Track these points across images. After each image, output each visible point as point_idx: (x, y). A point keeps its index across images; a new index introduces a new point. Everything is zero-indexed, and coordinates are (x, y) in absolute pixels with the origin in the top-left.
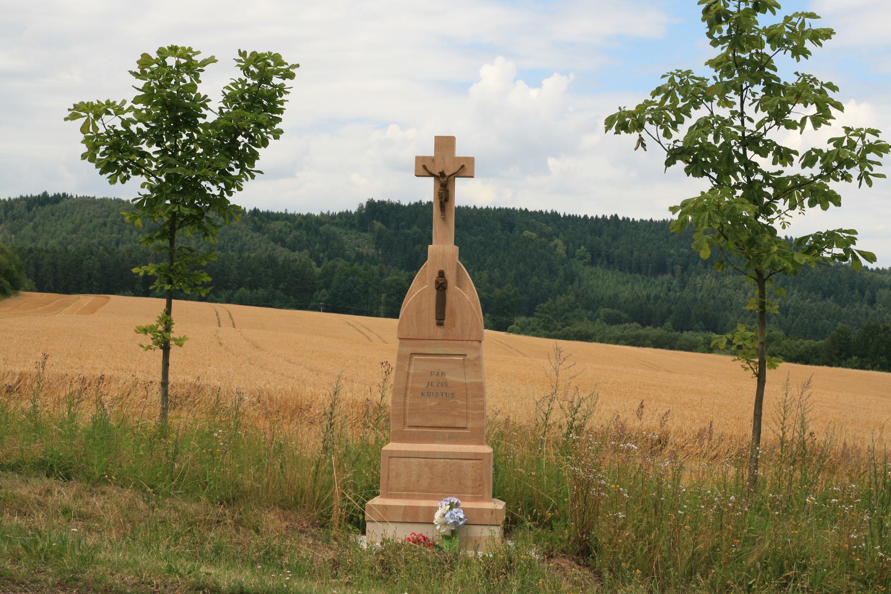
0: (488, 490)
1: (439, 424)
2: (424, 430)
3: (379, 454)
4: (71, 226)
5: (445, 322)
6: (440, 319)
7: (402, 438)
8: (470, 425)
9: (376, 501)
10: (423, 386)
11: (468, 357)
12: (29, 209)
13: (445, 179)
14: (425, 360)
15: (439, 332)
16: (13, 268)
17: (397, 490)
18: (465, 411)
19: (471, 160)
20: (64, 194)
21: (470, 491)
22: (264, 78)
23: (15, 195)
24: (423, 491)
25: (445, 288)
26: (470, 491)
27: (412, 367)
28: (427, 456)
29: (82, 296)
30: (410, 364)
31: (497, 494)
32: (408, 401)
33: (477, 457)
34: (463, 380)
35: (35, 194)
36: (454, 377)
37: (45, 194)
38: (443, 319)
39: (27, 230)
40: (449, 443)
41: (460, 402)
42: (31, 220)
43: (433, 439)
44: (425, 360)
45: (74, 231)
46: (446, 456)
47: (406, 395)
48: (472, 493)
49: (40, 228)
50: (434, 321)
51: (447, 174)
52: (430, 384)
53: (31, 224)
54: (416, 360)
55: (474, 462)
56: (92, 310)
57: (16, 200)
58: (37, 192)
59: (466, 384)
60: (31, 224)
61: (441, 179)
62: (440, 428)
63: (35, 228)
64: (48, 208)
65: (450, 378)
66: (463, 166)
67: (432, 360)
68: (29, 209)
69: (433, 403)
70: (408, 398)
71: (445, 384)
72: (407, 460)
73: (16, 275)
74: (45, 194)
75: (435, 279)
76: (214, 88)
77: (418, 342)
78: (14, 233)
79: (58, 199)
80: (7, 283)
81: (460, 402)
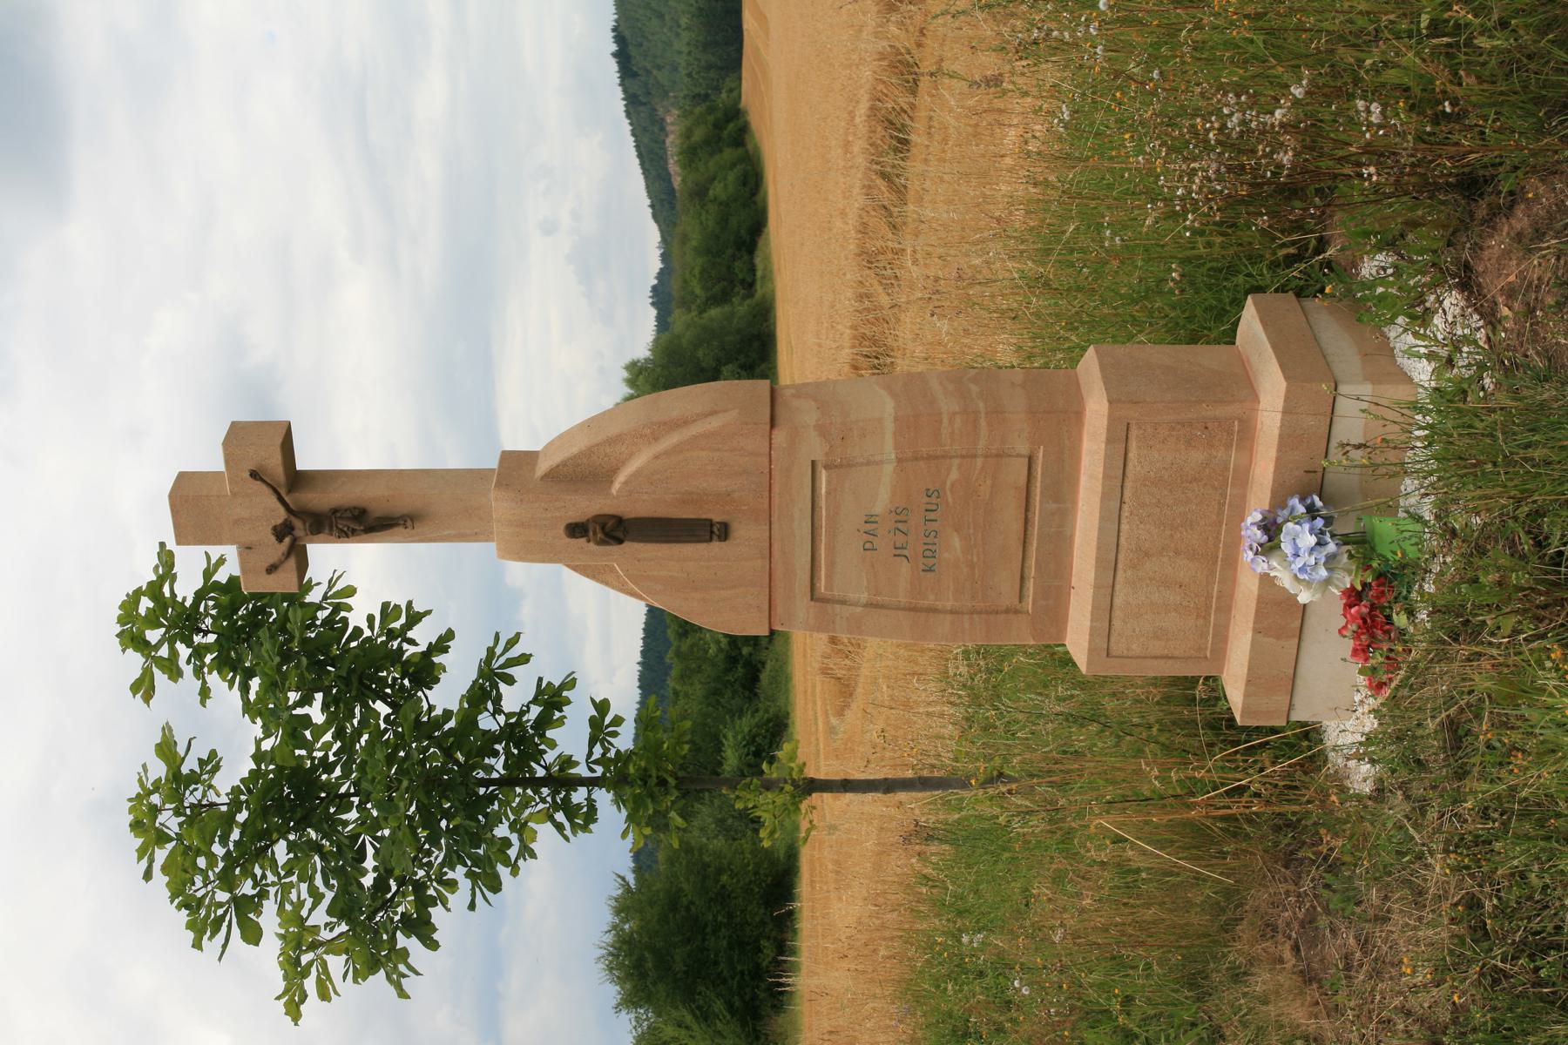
0: (1208, 356)
1: (1017, 526)
2: (1032, 562)
3: (1102, 681)
4: (655, 22)
5: (716, 518)
6: (712, 531)
7: (1055, 613)
8: (1023, 448)
9: (1235, 696)
10: (905, 568)
11: (819, 456)
12: (635, 75)
13: (297, 523)
14: (831, 565)
15: (746, 533)
16: (711, 118)
17: (1204, 635)
18: (979, 462)
19: (238, 436)
20: (614, 30)
21: (1221, 454)
22: (185, 622)
23: (619, 93)
24: (1213, 573)
25: (620, 521)
26: (1221, 454)
27: (851, 596)
28: (1109, 565)
29: (745, 26)
30: (843, 602)
31: (1217, 325)
32: (948, 605)
33: (1113, 377)
34: (889, 469)
35: (615, 67)
36: (880, 490)
37: (614, 55)
38: (711, 523)
39: (662, 77)
40: (1074, 502)
41: (954, 475)
42: (649, 72)
43: (1059, 545)
44: (831, 565)
45: (661, 16)
46: (1113, 515)
47: (933, 610)
48: (1229, 446)
49: (658, 61)
50: (716, 546)
51: (281, 515)
52: (899, 552)
53: (655, 72)
54: (829, 587)
55: (1133, 445)
56: (762, 18)
57: (625, 91)
58: (613, 66)
59: (899, 461)
60: (655, 72)
61: (299, 532)
62: (1027, 521)
63: (659, 68)
64: (633, 51)
65: (882, 502)
66: (254, 475)
67: (831, 550)
68: (635, 75)
69: (956, 542)
70: (939, 604)
71: (900, 514)
72: (1117, 613)
73: (719, 114)
74: (614, 55)
75: (592, 546)
76: (227, 731)
77: (779, 584)
78: (666, 93)
79: (620, 38)
80: (731, 126)
81: (954, 475)
